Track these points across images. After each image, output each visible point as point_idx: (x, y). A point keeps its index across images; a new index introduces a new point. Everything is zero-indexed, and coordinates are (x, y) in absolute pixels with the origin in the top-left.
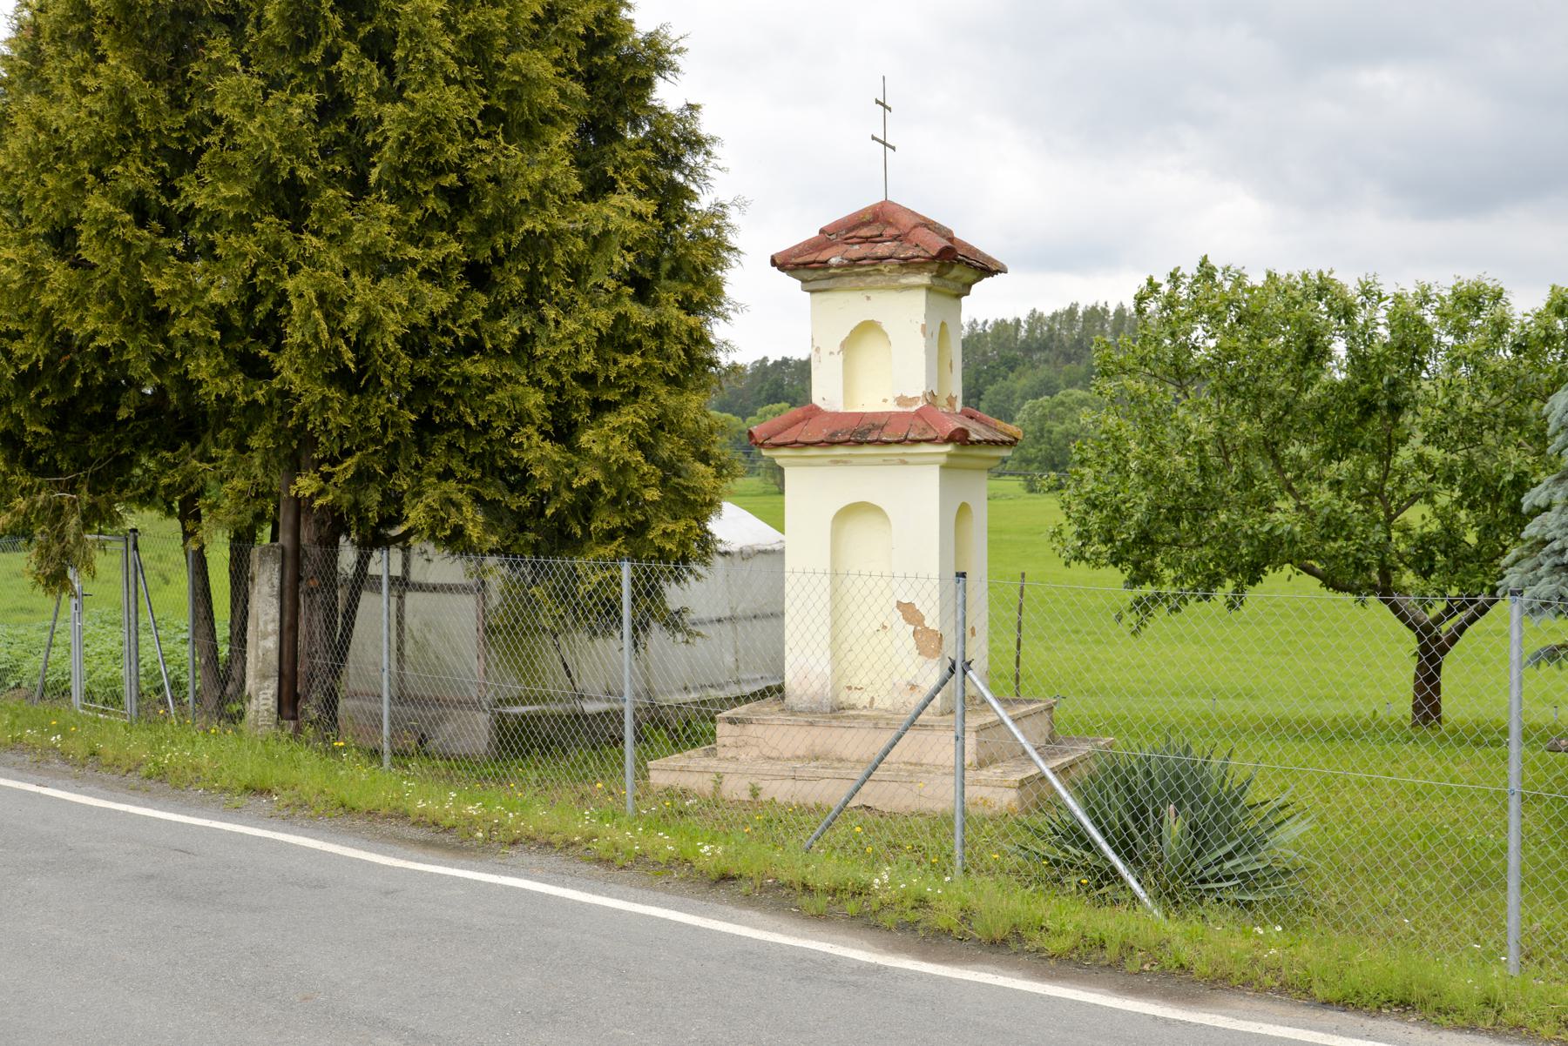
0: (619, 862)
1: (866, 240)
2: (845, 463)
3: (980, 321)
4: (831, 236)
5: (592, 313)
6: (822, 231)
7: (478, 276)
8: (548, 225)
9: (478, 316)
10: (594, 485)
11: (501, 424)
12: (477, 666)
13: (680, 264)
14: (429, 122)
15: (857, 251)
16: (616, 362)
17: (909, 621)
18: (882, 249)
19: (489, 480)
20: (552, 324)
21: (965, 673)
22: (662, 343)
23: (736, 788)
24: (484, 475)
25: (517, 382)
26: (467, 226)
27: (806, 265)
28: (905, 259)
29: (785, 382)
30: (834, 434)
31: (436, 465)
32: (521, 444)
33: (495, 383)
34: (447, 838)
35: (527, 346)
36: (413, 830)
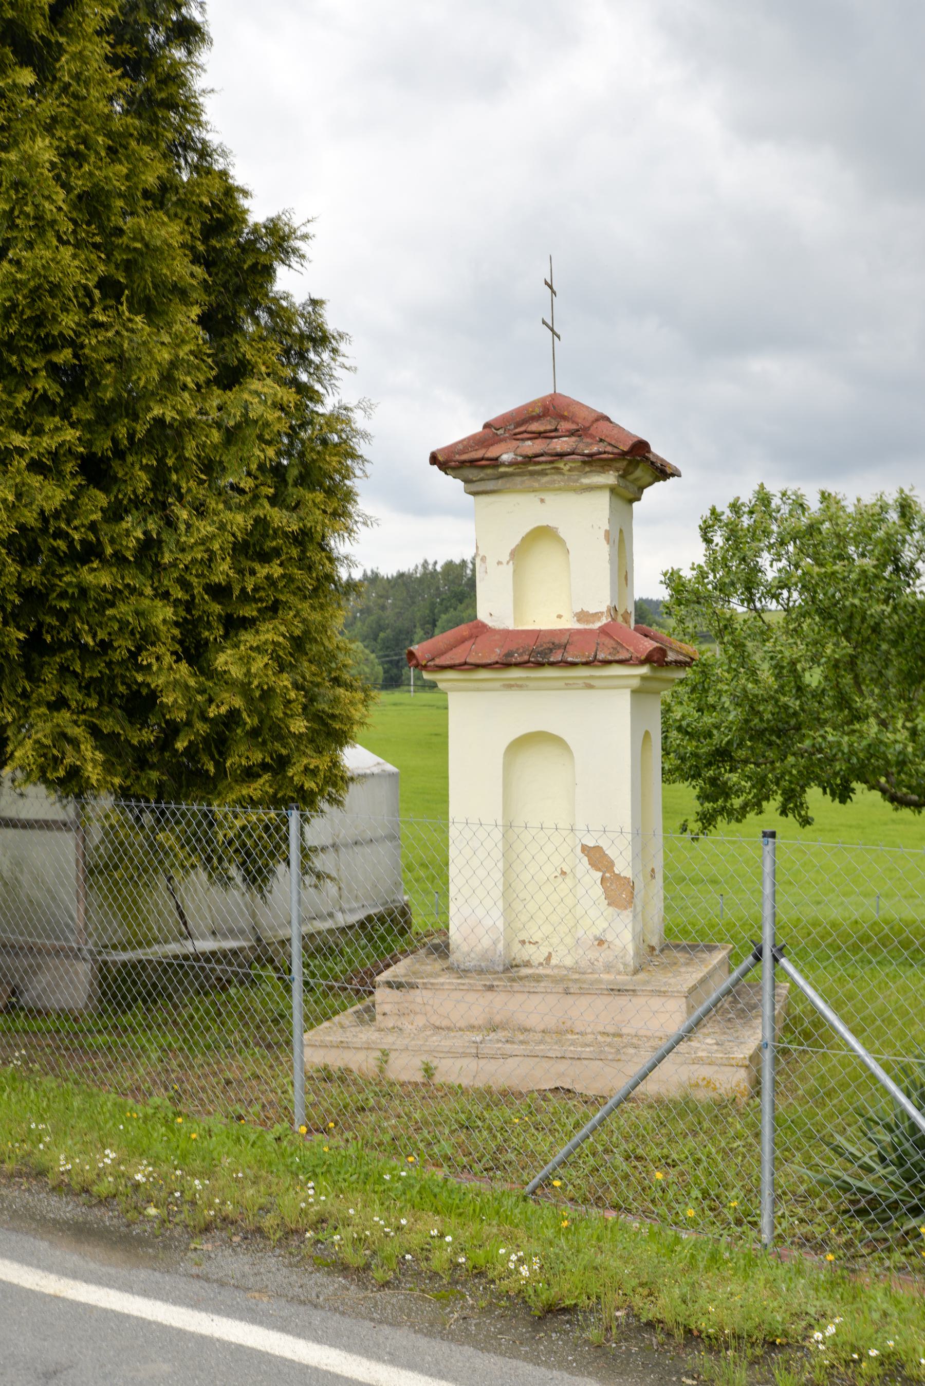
0: (379, 1275)
1: (539, 435)
2: (520, 687)
3: (431, 562)
4: (494, 431)
5: (229, 515)
6: (487, 426)
7: (96, 471)
8: (179, 412)
9: (97, 516)
10: (233, 715)
11: (124, 644)
12: (76, 911)
13: (313, 469)
14: (39, 287)
15: (530, 447)
16: (253, 572)
17: (594, 865)
18: (561, 444)
19: (106, 709)
20: (183, 527)
21: (776, 960)
22: (303, 552)
23: (406, 1068)
24: (100, 704)
25: (141, 594)
26: (82, 412)
27: (472, 463)
28: (590, 455)
29: (448, 593)
30: (510, 654)
31: (46, 692)
32: (150, 666)
33: (116, 594)
34: (106, 1217)
35: (152, 553)
36: (54, 1200)
